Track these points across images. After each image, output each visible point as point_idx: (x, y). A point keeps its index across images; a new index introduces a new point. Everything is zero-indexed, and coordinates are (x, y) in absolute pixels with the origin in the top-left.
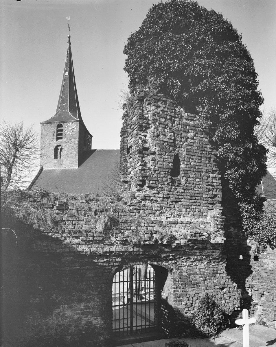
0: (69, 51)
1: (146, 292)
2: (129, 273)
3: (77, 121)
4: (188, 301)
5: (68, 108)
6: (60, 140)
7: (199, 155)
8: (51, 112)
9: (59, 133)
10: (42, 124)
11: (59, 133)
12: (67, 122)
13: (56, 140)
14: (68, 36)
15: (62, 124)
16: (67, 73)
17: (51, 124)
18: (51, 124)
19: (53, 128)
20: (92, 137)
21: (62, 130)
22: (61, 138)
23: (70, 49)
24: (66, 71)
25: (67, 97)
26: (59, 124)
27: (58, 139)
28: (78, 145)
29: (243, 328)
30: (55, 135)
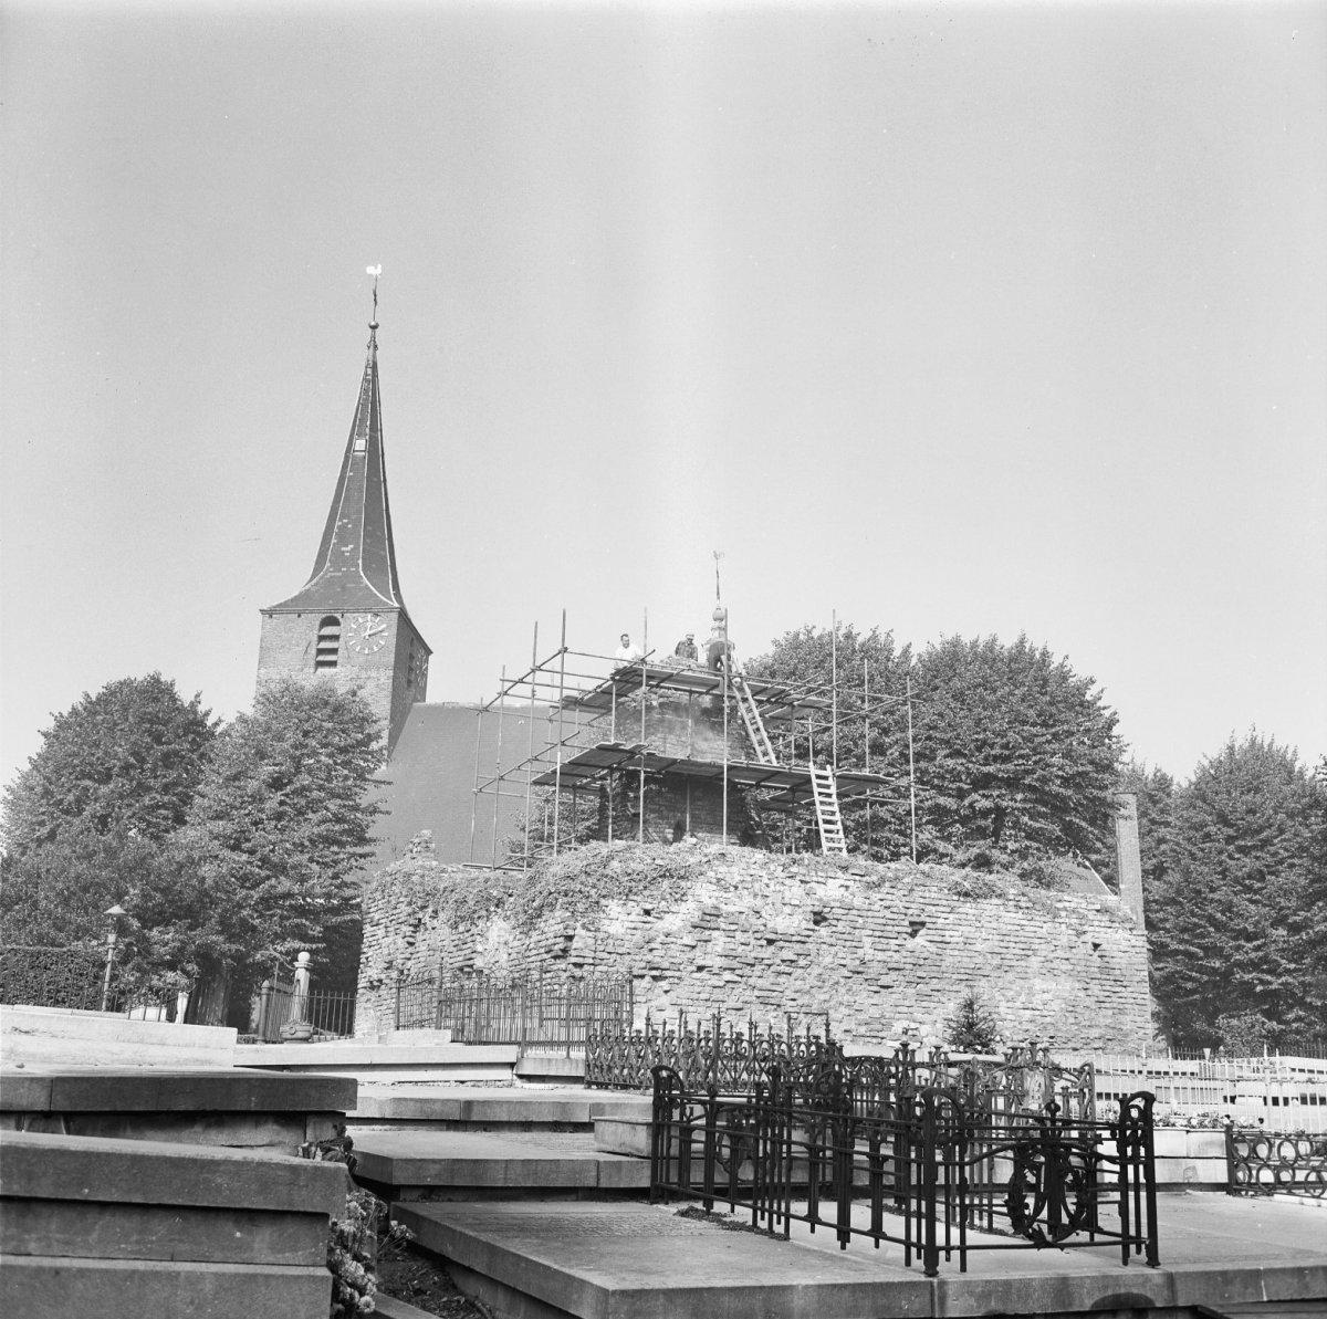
0: (369, 371)
1: (1114, 1179)
2: (286, 1073)
3: (392, 609)
4: (82, 988)
5: (360, 562)
6: (321, 670)
7: (467, 1004)
8: (294, 574)
9: (324, 645)
10: (269, 613)
11: (324, 645)
12: (357, 611)
13: (312, 670)
14: (373, 323)
15: (338, 616)
16: (360, 444)
17: (299, 616)
18: (299, 616)
19: (306, 629)
20: (429, 652)
21: (336, 638)
22: (333, 664)
23: (375, 367)
24: (360, 435)
25: (356, 524)
26: (327, 617)
27: (320, 664)
28: (390, 689)
29: (1078, 1066)
30: (314, 652)
